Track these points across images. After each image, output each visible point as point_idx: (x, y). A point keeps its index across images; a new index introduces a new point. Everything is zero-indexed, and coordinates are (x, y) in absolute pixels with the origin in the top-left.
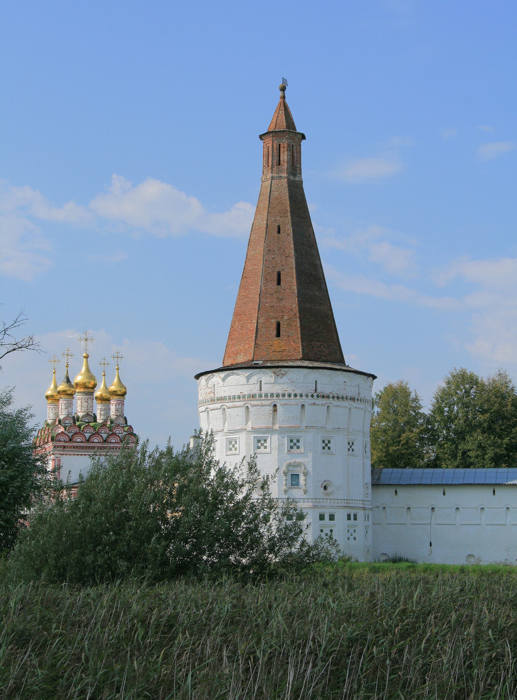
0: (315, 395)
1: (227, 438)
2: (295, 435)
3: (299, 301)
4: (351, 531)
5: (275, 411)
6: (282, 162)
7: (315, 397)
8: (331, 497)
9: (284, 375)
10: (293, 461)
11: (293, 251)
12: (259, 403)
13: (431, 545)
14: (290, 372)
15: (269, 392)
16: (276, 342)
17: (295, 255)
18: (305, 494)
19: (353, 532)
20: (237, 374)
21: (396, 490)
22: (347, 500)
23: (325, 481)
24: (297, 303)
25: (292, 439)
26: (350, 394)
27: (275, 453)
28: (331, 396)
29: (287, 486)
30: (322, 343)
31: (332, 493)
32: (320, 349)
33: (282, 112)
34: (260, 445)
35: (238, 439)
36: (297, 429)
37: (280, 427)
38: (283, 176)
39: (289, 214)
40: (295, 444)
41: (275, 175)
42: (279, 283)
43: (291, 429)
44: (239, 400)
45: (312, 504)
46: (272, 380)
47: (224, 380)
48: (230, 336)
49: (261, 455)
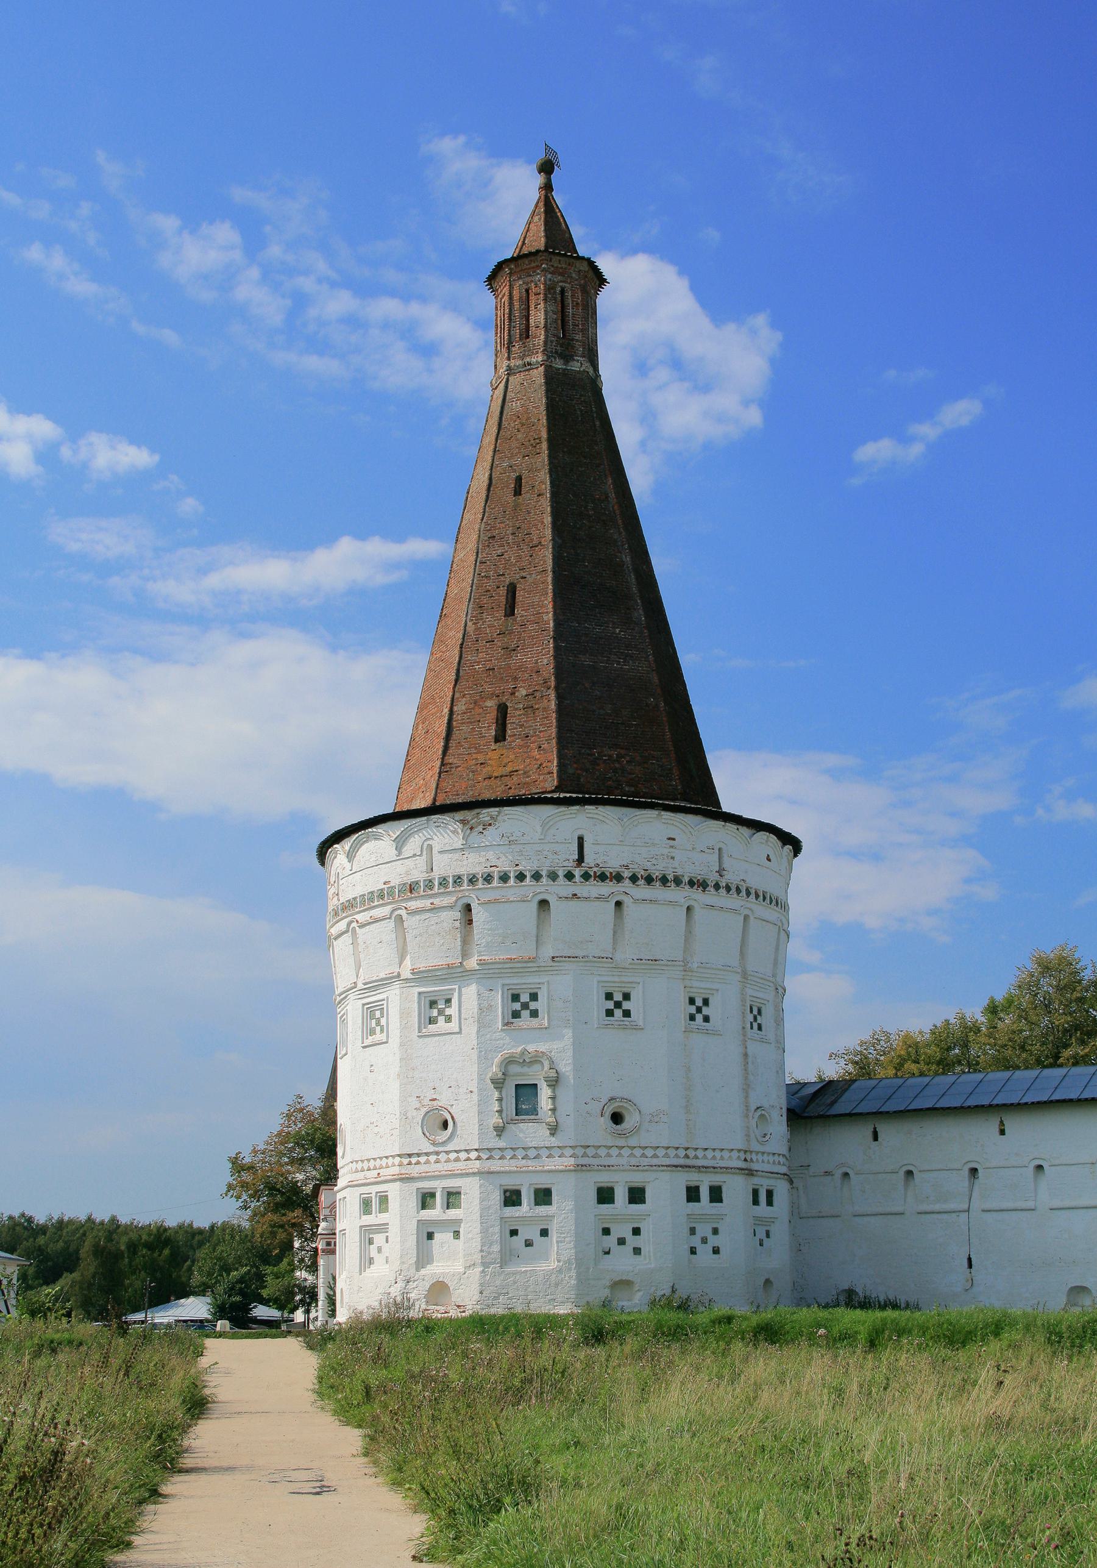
0: (577, 873)
1: (364, 1005)
2: (523, 981)
3: (556, 648)
4: (704, 1230)
5: (470, 922)
6: (532, 332)
7: (577, 878)
8: (633, 1142)
9: (490, 825)
10: (519, 1049)
11: (548, 533)
12: (426, 903)
13: (970, 1266)
14: (506, 818)
15: (450, 873)
16: (495, 756)
17: (553, 539)
18: (552, 1134)
19: (708, 1233)
20: (377, 838)
21: (875, 1128)
22: (687, 1149)
23: (612, 1099)
24: (552, 653)
25: (515, 992)
26: (687, 871)
27: (471, 1029)
28: (626, 874)
29: (504, 1115)
30: (623, 752)
31: (636, 1130)
32: (617, 765)
33: (540, 219)
34: (435, 1013)
35: (385, 1002)
36: (528, 964)
37: (481, 963)
38: (534, 360)
39: (545, 445)
40: (525, 1006)
41: (513, 363)
42: (510, 611)
43: (511, 966)
44: (381, 902)
45: (572, 1161)
46: (458, 842)
47: (351, 856)
48: (407, 761)
49: (437, 1038)
